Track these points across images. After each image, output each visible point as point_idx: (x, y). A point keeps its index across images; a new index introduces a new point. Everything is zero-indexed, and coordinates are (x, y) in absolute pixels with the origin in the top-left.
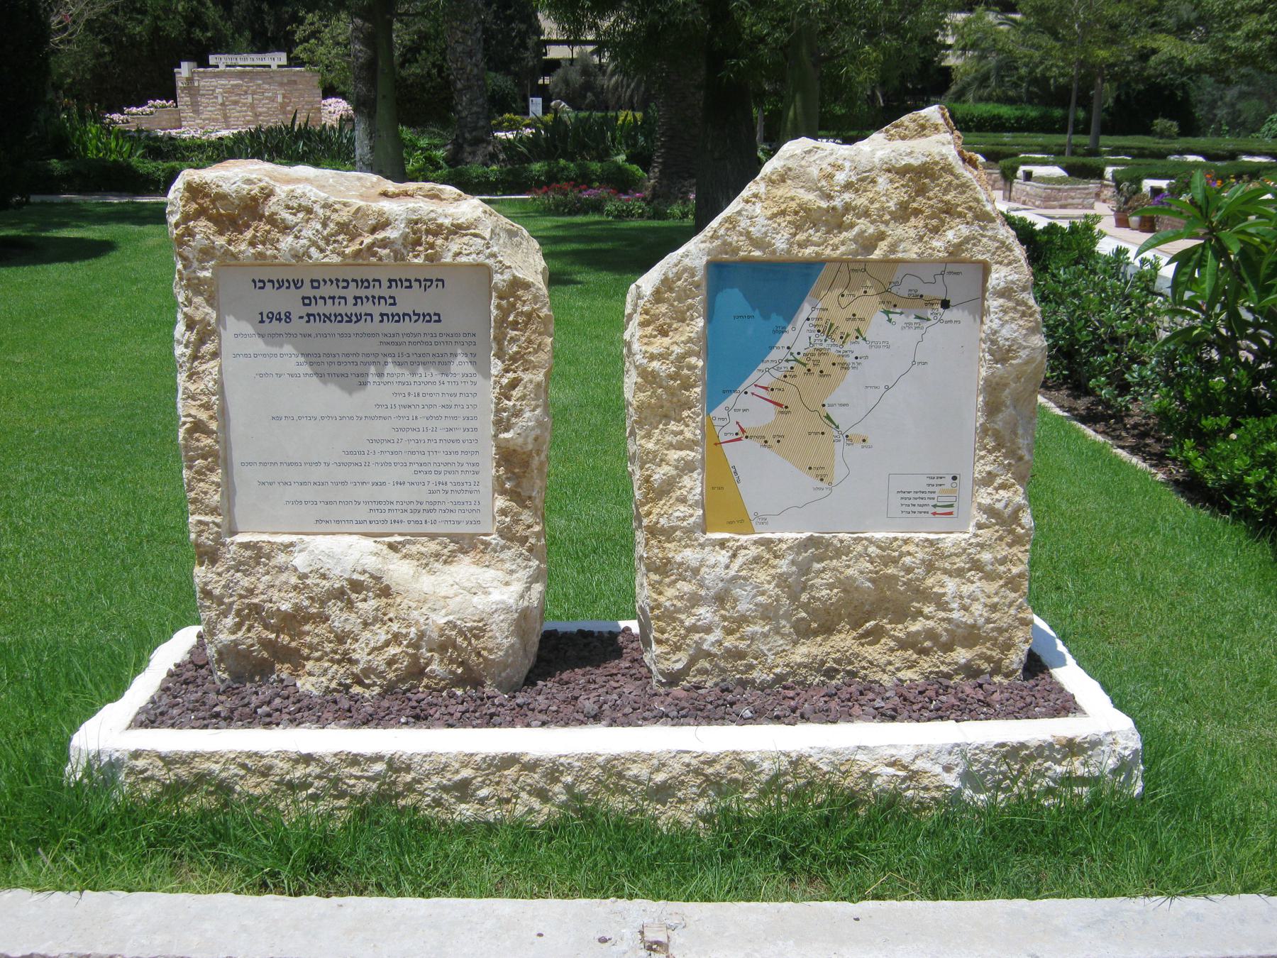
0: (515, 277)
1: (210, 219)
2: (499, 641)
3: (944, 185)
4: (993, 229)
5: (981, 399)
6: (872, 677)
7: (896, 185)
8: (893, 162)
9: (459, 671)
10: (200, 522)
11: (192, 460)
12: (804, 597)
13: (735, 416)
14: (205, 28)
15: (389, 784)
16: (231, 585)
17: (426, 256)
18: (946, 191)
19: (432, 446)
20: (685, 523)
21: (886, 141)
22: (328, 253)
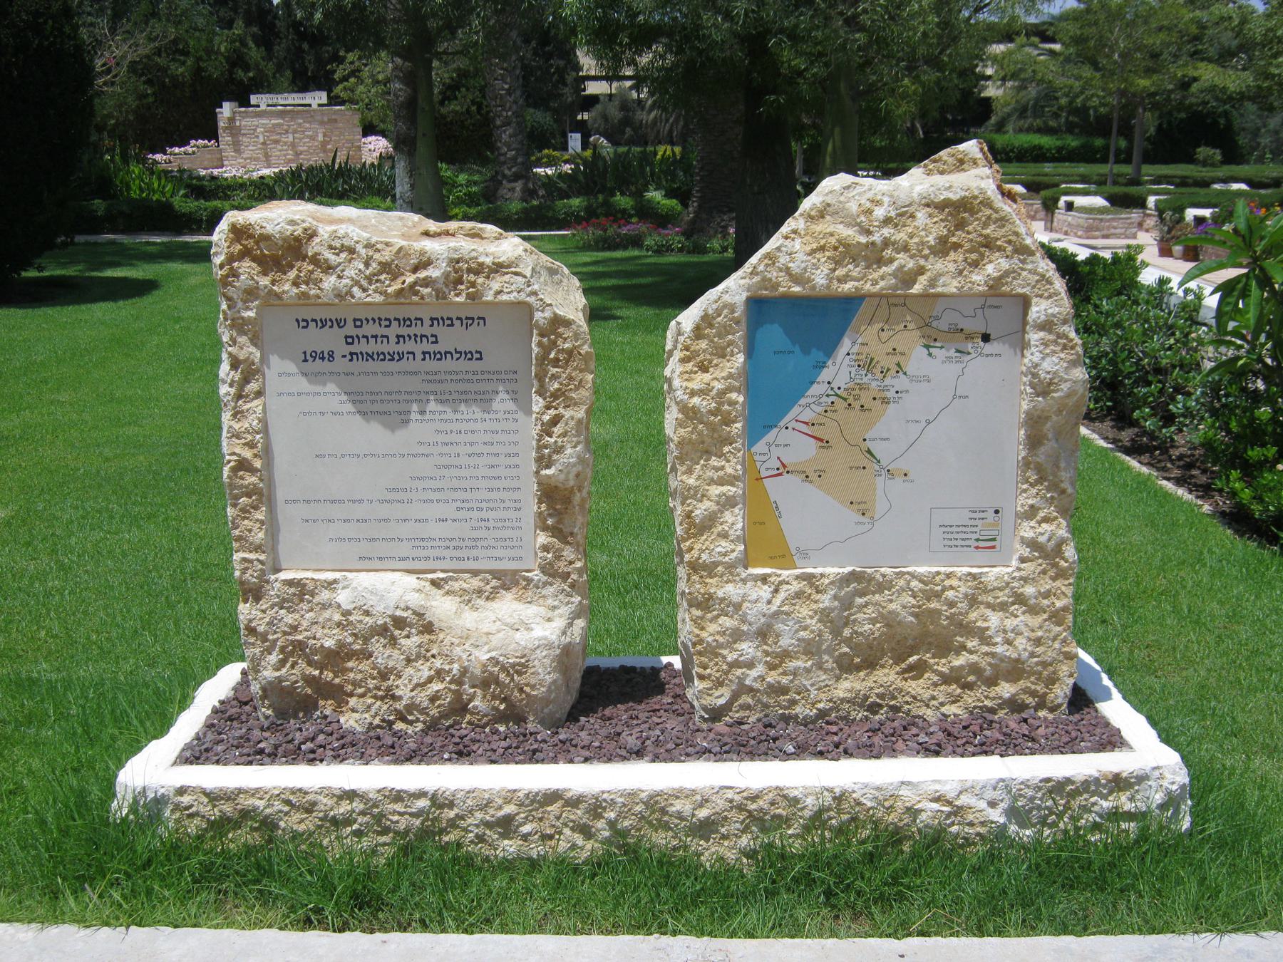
2: (541, 677)
3: (983, 219)
4: (1032, 262)
5: (1022, 432)
6: (915, 712)
7: (935, 219)
8: (932, 196)
9: (502, 707)
10: (244, 560)
11: (237, 497)
12: (847, 632)
13: (776, 452)
14: (247, 68)
17: (468, 294)
18: (985, 225)
20: (727, 559)
21: (925, 176)
22: (370, 292)
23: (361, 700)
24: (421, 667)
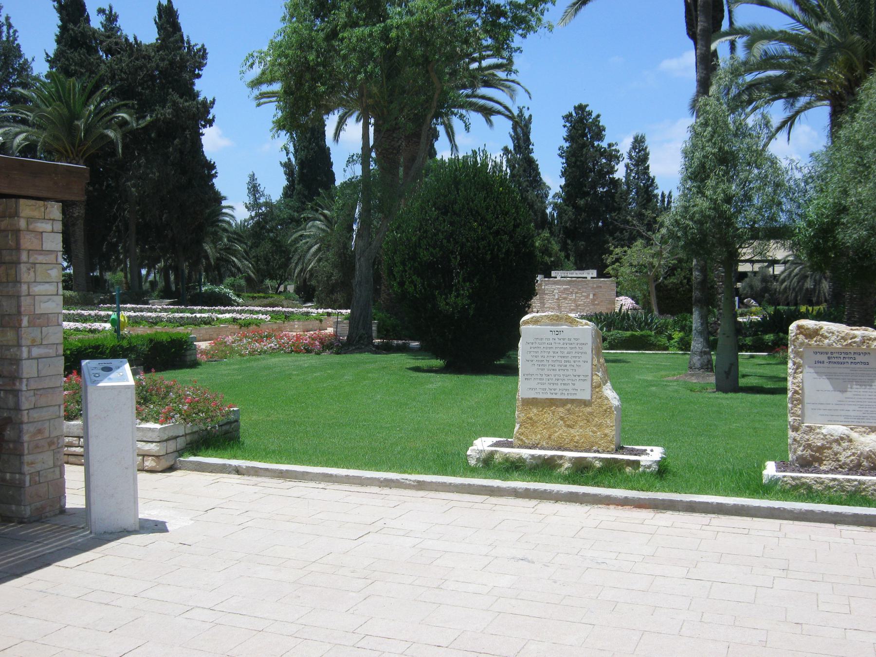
14: (550, 256)
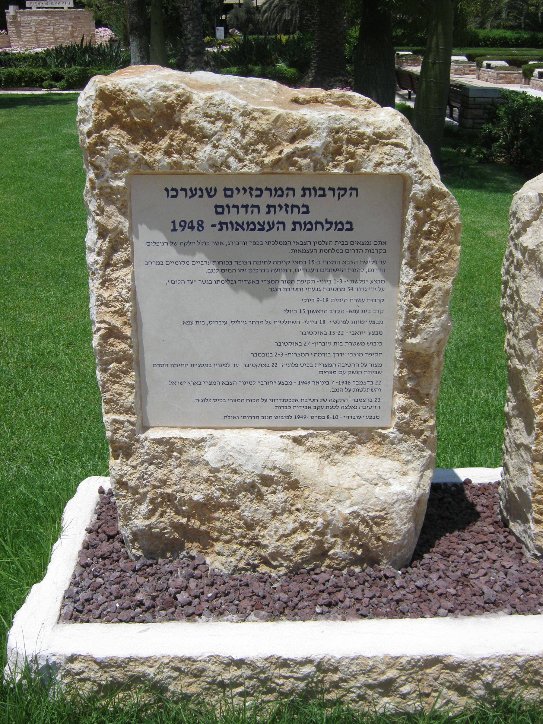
0: (432, 187)
1: (123, 127)
2: (398, 527)
9: (359, 552)
10: (115, 421)
11: (107, 363)
15: (315, 683)
16: (145, 476)
17: (346, 165)
19: (338, 349)
22: (247, 162)
23: (227, 545)
24: (287, 520)
